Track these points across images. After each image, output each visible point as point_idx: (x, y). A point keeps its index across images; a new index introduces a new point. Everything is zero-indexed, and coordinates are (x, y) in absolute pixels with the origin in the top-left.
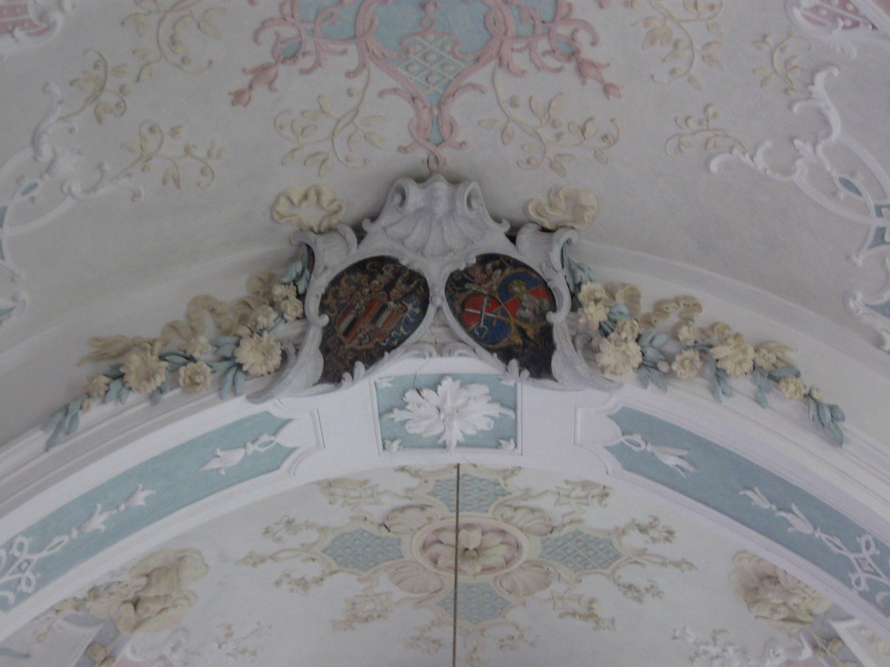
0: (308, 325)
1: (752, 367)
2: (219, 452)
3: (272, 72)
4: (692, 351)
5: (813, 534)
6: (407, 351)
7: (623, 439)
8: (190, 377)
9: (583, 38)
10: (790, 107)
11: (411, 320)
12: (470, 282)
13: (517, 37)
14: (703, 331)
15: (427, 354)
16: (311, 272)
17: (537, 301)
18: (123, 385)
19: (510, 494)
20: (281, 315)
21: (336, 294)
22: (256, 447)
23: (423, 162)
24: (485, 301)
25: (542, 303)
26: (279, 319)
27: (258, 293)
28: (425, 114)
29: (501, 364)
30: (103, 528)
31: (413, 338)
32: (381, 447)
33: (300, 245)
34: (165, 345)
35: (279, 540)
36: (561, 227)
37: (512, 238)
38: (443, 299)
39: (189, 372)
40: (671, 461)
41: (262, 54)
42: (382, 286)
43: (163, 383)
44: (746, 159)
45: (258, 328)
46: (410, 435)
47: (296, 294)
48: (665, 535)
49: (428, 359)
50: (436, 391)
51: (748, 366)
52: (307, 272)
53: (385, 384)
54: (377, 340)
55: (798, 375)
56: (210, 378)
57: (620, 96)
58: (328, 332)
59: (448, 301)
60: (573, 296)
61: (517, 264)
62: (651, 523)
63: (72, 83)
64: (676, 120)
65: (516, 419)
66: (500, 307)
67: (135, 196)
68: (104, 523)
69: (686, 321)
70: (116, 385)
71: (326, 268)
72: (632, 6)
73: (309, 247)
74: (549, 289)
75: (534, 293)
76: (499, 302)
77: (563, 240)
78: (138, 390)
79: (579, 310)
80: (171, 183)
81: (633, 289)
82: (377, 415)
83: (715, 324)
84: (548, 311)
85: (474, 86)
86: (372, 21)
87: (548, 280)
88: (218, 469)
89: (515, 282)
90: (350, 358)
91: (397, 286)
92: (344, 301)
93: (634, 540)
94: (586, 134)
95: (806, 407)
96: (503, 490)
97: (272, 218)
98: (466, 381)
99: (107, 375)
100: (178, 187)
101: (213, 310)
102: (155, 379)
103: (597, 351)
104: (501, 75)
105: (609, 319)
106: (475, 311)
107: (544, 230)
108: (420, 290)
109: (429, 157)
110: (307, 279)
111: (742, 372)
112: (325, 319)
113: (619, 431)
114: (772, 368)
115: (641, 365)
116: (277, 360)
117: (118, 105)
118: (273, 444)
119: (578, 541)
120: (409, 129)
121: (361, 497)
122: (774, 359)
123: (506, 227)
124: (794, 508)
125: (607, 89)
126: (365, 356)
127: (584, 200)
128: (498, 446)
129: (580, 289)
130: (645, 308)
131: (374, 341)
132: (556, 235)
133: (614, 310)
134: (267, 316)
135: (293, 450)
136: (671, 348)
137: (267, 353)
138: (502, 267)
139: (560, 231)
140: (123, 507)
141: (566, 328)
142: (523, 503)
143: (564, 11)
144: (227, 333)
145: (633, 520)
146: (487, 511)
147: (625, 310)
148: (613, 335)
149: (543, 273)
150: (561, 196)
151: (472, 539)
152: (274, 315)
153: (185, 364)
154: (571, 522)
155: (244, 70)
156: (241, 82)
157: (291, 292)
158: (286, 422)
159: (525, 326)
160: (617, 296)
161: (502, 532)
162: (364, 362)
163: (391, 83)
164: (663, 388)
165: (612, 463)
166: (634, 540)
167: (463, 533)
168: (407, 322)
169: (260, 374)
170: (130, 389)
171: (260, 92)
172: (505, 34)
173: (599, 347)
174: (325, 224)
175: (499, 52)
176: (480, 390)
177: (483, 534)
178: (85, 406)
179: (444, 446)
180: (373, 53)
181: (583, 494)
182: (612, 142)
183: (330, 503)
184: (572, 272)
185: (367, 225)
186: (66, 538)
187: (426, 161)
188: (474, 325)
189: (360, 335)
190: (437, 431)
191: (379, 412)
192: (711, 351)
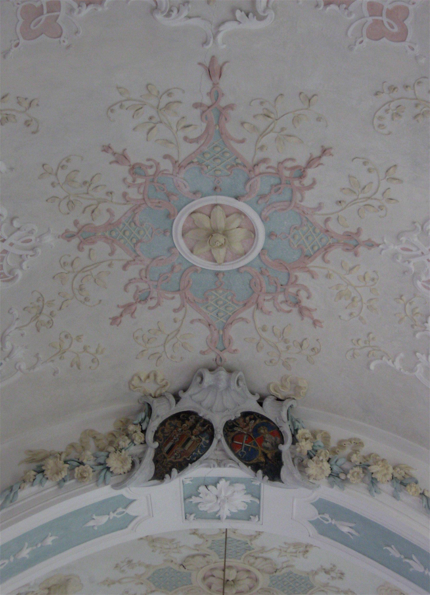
0: (147, 448)
1: (392, 478)
2: (94, 517)
3: (134, 307)
4: (359, 468)
5: (424, 572)
6: (201, 463)
7: (319, 517)
8: (81, 474)
9: (303, 294)
10: (414, 335)
11: (204, 446)
12: (237, 427)
13: (267, 293)
14: (364, 457)
15: (212, 465)
16: (150, 419)
17: (273, 438)
18: (44, 476)
19: (253, 549)
20: (132, 441)
21: (163, 431)
22: (115, 515)
23: (213, 360)
24: (245, 438)
25: (276, 439)
26: (131, 443)
27: (120, 429)
28: (216, 334)
29: (252, 472)
30: (28, 557)
31: (204, 457)
32: (184, 517)
33: (144, 403)
34: (67, 456)
35: (123, 571)
36: (288, 398)
37: (260, 403)
38: (222, 435)
39: (80, 471)
40: (345, 529)
41: (129, 298)
42: (189, 427)
43: (65, 476)
44: (390, 363)
45: (120, 448)
46: (201, 511)
47: (141, 430)
48: (339, 575)
49: (212, 468)
50: (216, 487)
51: (389, 477)
52: (147, 418)
53: (188, 482)
54: (185, 457)
55: (417, 483)
56: (92, 475)
57: (321, 327)
58: (158, 451)
59: (224, 436)
60: (293, 436)
61: (262, 417)
62: (331, 568)
63: (24, 309)
64: (352, 340)
65: (260, 503)
66: (253, 441)
67: (55, 373)
68: (28, 554)
69: (356, 451)
70: (40, 476)
71: (158, 416)
72: (330, 278)
73: (149, 405)
74: (280, 432)
75: (273, 434)
76: (252, 438)
77: (288, 405)
78: (51, 479)
79: (297, 444)
80: (75, 366)
81: (326, 433)
82: (183, 499)
83: (372, 454)
84: (279, 444)
85: (243, 319)
86: (189, 282)
87: (280, 427)
88: (93, 526)
89: (262, 427)
90: (169, 466)
91: (197, 427)
92: (167, 435)
93: (322, 578)
94: (303, 347)
95: (421, 500)
96: (249, 547)
97: (129, 387)
98: (233, 481)
99: (35, 471)
100: (79, 369)
101: (94, 438)
102: (61, 474)
103: (306, 466)
104: (258, 314)
105: (313, 449)
106: (239, 443)
107: (278, 399)
108: (209, 430)
109: (217, 357)
110: (147, 422)
111: (386, 480)
112: (157, 444)
113: (317, 512)
114: (403, 479)
115: (330, 475)
116: (128, 466)
117: (48, 322)
118: (125, 513)
119: (291, 577)
120: (206, 342)
121: (170, 549)
122: (403, 474)
123: (257, 397)
124: (414, 557)
125: (315, 323)
126: (178, 466)
127: (301, 384)
128: (249, 519)
129: (297, 432)
130: (333, 444)
131: (183, 457)
132: (284, 403)
133: (316, 444)
134: (124, 442)
135: (135, 517)
136: (347, 466)
137: (123, 461)
138: (255, 419)
139: (287, 400)
140: (39, 545)
141: (289, 454)
142: (260, 555)
143: (293, 279)
144: (102, 450)
145: (322, 566)
146: (240, 559)
147: (322, 444)
148: (315, 458)
149: (277, 423)
150: (288, 381)
151: (231, 575)
152: (128, 441)
153: (78, 466)
154: (287, 567)
155: (118, 306)
156: (116, 312)
157: (138, 429)
158: (133, 501)
159: (266, 452)
160: (317, 437)
161: (248, 571)
162: (176, 468)
163: (198, 316)
164: (342, 488)
165: (312, 530)
166: (322, 578)
167: (227, 571)
168: (201, 447)
169: (119, 474)
170: (47, 479)
171: (126, 318)
172: (261, 291)
173: (307, 464)
174: (158, 393)
175: (257, 301)
176: (240, 487)
177: (237, 572)
178: (22, 487)
179: (219, 518)
180: (189, 300)
181: (294, 550)
182: (317, 352)
183: (153, 551)
184: (293, 423)
185: (181, 394)
186: (7, 561)
187: (215, 359)
188: (238, 451)
189: (176, 454)
190: (216, 510)
191: (184, 497)
192: (369, 468)
